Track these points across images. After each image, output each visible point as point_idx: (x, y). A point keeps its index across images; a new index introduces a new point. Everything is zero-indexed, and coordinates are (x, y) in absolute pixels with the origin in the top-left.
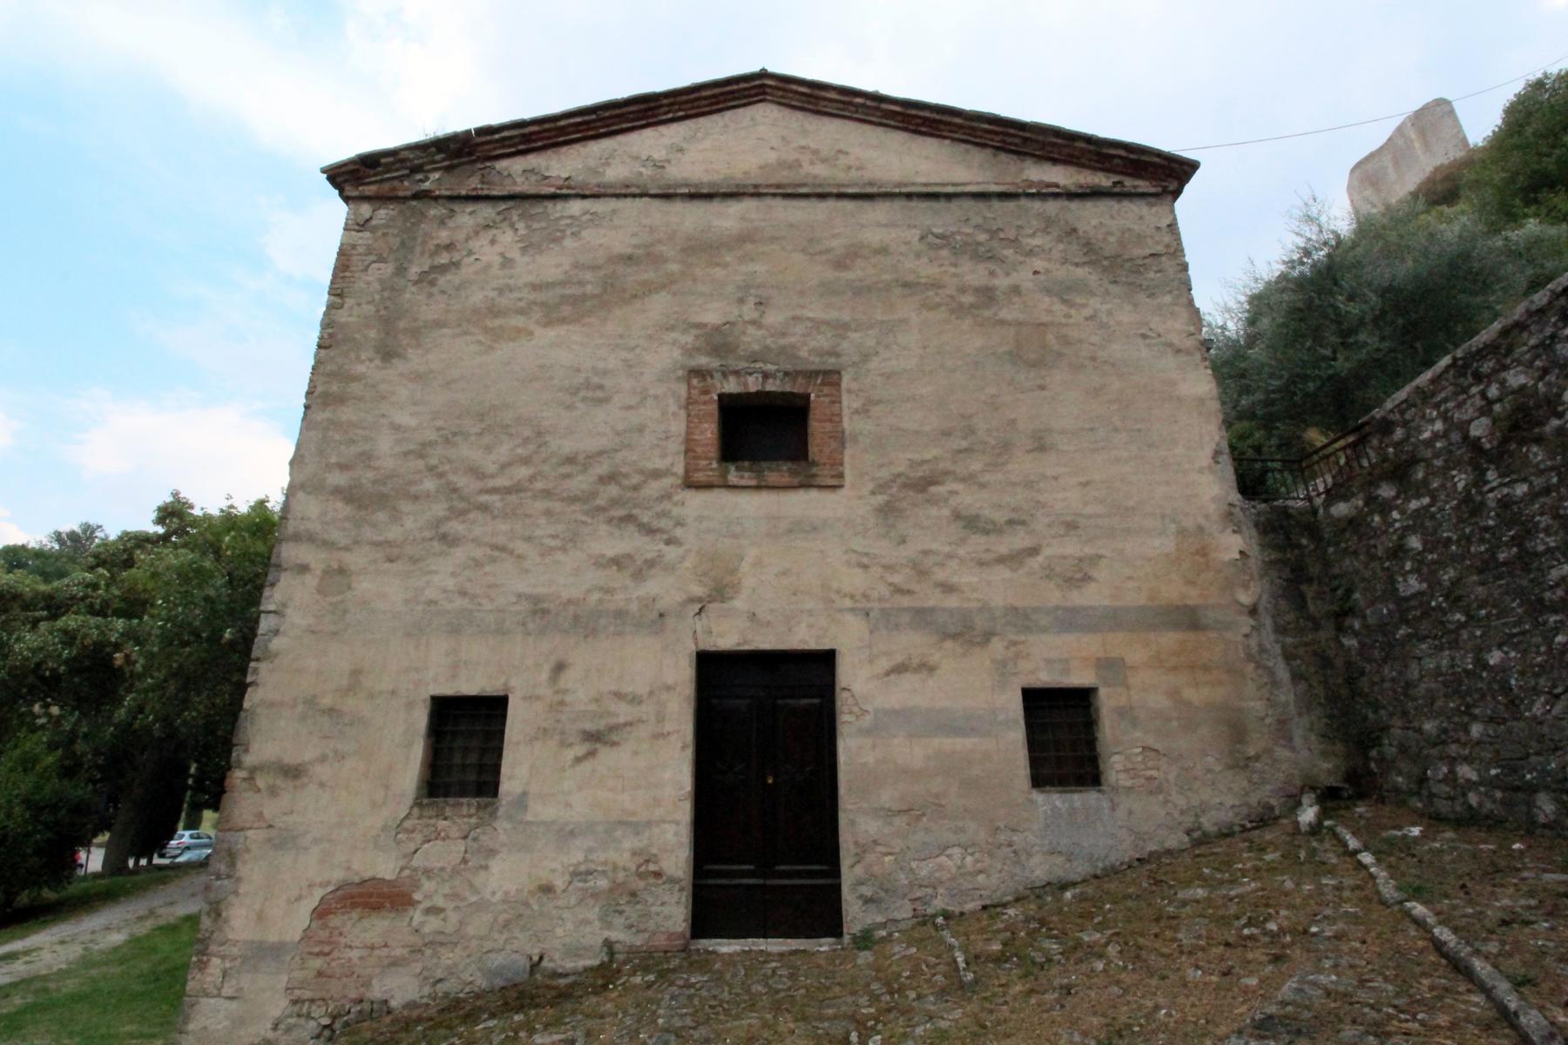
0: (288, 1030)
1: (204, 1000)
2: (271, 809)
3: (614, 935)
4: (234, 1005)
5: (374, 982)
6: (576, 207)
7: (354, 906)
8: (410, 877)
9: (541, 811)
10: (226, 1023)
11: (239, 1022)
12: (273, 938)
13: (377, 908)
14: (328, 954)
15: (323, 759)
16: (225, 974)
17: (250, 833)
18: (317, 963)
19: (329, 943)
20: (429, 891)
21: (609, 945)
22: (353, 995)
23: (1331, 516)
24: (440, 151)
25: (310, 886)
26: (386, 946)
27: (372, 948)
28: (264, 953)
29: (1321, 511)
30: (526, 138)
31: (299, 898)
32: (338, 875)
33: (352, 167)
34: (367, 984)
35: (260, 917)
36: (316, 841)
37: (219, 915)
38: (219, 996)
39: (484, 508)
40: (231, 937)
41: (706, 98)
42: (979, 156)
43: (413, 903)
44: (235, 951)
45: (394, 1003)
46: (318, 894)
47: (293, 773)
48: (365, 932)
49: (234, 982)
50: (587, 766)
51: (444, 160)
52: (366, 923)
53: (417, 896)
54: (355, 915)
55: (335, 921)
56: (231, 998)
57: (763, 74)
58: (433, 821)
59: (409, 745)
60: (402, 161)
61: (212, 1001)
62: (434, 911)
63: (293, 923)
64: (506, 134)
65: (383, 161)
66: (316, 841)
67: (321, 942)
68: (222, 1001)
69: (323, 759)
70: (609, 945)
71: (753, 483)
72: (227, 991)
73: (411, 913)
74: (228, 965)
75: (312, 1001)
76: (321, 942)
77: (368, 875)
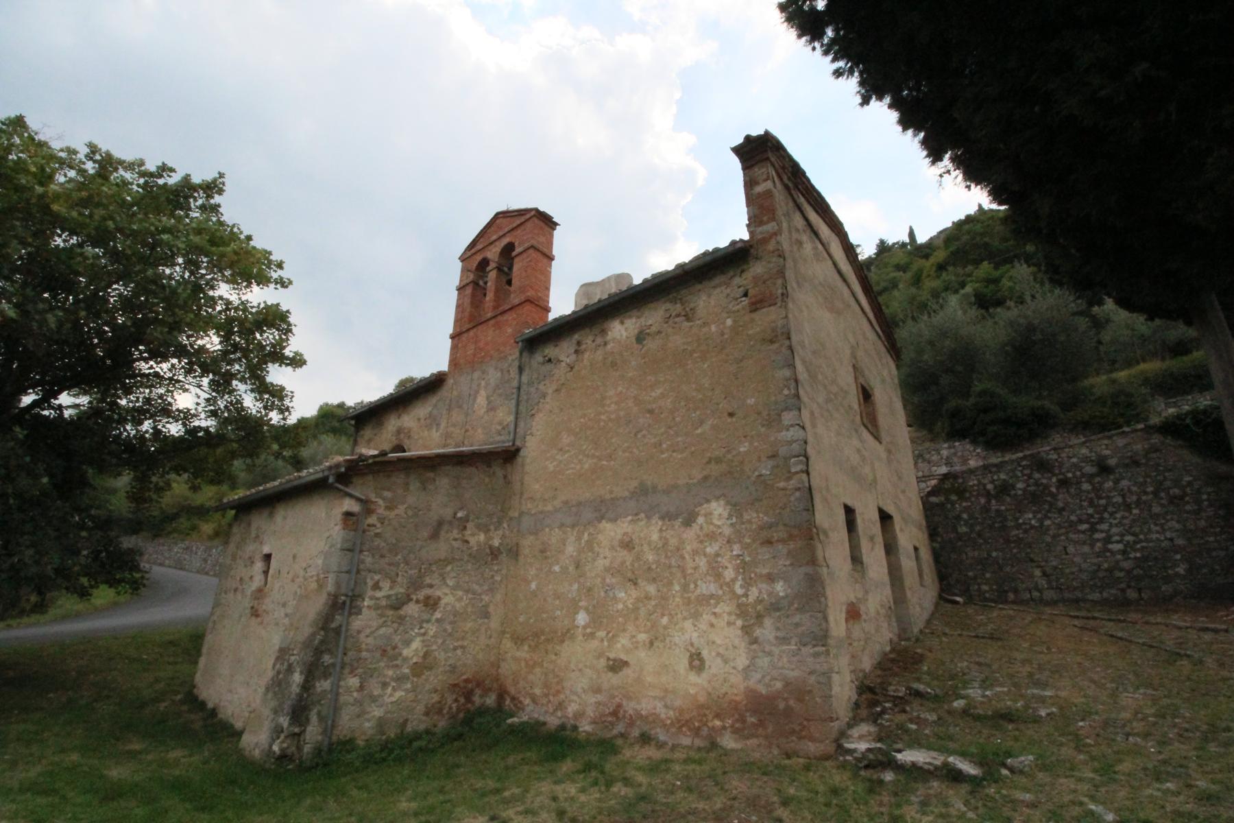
57: (841, 224)
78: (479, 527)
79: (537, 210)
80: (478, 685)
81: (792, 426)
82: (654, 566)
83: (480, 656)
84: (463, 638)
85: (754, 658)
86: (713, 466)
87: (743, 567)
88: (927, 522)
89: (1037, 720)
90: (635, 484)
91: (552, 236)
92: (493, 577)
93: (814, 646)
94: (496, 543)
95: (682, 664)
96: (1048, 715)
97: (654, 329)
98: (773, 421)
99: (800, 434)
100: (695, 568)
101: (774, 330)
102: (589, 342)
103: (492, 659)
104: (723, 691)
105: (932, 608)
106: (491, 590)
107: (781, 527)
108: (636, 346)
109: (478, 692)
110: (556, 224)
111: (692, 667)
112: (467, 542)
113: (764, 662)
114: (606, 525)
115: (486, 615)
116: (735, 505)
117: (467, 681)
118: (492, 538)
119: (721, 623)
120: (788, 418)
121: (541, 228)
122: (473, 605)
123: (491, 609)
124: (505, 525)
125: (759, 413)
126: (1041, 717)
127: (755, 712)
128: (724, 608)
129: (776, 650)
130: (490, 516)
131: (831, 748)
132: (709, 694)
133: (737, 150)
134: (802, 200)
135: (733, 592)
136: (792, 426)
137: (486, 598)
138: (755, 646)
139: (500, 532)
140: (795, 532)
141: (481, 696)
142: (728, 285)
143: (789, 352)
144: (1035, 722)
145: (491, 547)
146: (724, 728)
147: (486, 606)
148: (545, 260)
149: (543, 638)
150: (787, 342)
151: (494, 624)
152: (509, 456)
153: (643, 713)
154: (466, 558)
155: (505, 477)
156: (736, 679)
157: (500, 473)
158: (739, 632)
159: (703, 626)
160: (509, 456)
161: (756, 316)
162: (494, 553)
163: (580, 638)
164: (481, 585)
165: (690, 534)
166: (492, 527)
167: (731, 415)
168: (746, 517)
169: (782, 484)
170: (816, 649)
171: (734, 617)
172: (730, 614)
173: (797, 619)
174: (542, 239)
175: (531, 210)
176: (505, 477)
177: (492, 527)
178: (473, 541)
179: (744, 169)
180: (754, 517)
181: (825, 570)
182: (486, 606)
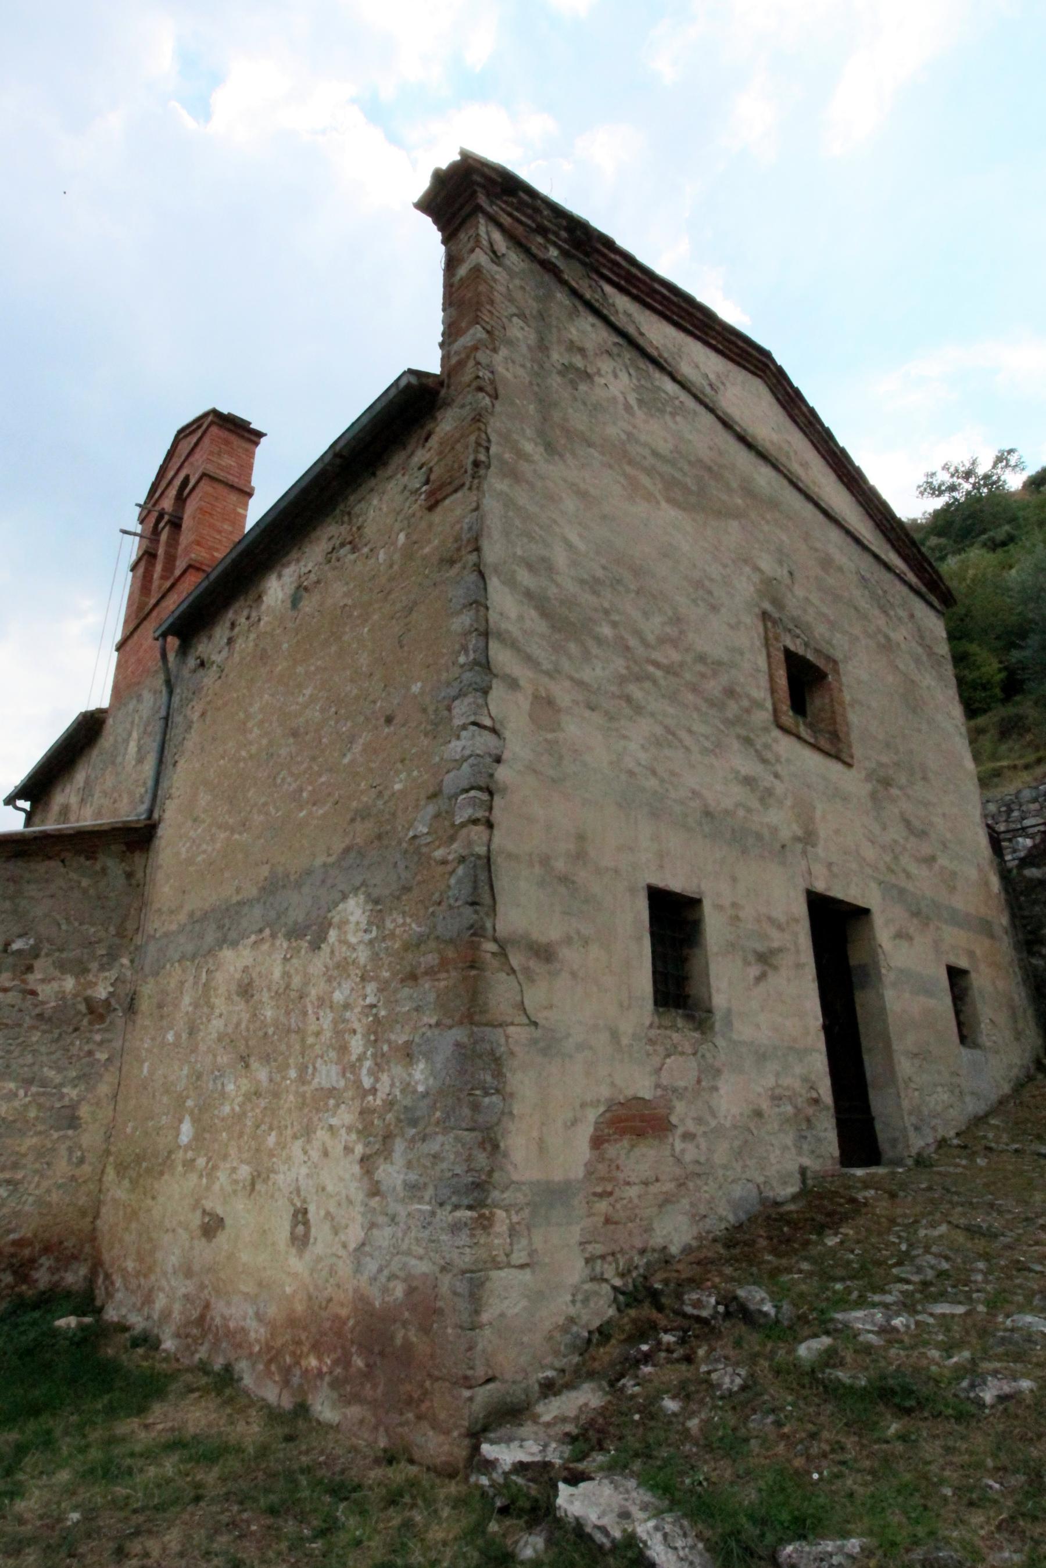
0: (586, 1301)
1: (494, 1274)
2: (534, 997)
3: (806, 1161)
4: (526, 1276)
5: (655, 1225)
6: (670, 387)
7: (623, 1132)
8: (662, 1096)
9: (743, 1031)
10: (524, 1303)
11: (537, 1297)
12: (558, 1176)
13: (640, 1134)
14: (611, 1194)
15: (568, 940)
16: (513, 1232)
17: (511, 1030)
18: (602, 1206)
19: (610, 1179)
20: (681, 1113)
21: (803, 1171)
22: (639, 1244)
23: (1025, 877)
24: (567, 229)
25: (583, 1105)
26: (657, 1180)
27: (646, 1184)
28: (553, 1195)
29: (1015, 871)
30: (629, 277)
31: (574, 1122)
32: (605, 1092)
33: (494, 176)
34: (648, 1230)
35: (542, 1146)
36: (580, 1047)
37: (496, 1147)
38: (509, 1265)
39: (649, 677)
40: (515, 1177)
41: (738, 347)
42: (870, 524)
43: (670, 1127)
44: (521, 1198)
45: (674, 1250)
46: (592, 1115)
47: (545, 953)
48: (640, 1160)
49: (524, 1242)
50: (762, 987)
51: (565, 241)
52: (637, 1152)
53: (674, 1119)
54: (625, 1143)
55: (611, 1150)
56: (522, 1267)
57: (767, 354)
58: (668, 1032)
59: (639, 939)
60: (537, 210)
61: (502, 1274)
62: (688, 1136)
63: (572, 1156)
64: (618, 258)
65: (522, 194)
66: (580, 1047)
67: (602, 1179)
68: (513, 1271)
69: (568, 940)
70: (803, 1171)
71: (812, 741)
72: (519, 1257)
73: (671, 1140)
74: (515, 1219)
75: (603, 1257)
76: (602, 1179)
77: (630, 1093)
78: (63, 967)
79: (214, 412)
80: (47, 1250)
81: (464, 727)
82: (271, 1031)
83: (55, 1197)
84: (15, 1166)
85: (373, 1225)
86: (359, 826)
87: (377, 1030)
88: (1013, 916)
89: (967, 1413)
90: (265, 871)
91: (251, 455)
92: (90, 1053)
93: (456, 1207)
94: (101, 992)
95: (282, 1229)
96: (1002, 1398)
97: (313, 577)
98: (439, 726)
99: (484, 742)
100: (317, 1034)
101: (457, 539)
102: (243, 620)
103: (83, 1200)
104: (326, 1294)
105: (1007, 1088)
106: (83, 1077)
107: (432, 944)
108: (290, 613)
109: (46, 1262)
110: (260, 435)
111: (294, 1238)
112: (33, 993)
113: (384, 1236)
114: (226, 953)
115: (73, 1121)
116: (376, 902)
117: (19, 1243)
118: (92, 985)
119: (337, 1150)
120: (461, 712)
121: (227, 442)
122: (40, 1107)
123: (84, 1111)
124: (125, 961)
125: (424, 710)
126: (980, 1404)
127: (366, 1349)
128: (345, 1116)
129: (402, 1211)
130: (90, 944)
131: (461, 1453)
132: (310, 1298)
133: (430, 205)
134: (622, 303)
135: (358, 1084)
136: (464, 727)
137: (71, 1092)
138: (374, 1202)
139: (112, 974)
140: (451, 954)
141: (52, 1271)
142: (404, 469)
143: (474, 577)
144: (960, 1417)
145: (88, 1001)
146: (320, 1375)
147: (74, 1106)
148: (233, 497)
149: (144, 1166)
150: (473, 558)
151: (90, 1137)
152: (138, 838)
153: (232, 1325)
154: (28, 1021)
155: (129, 875)
156: (345, 1268)
157: (115, 868)
158: (356, 1169)
159: (315, 1155)
160: (138, 838)
161: (437, 517)
162: (97, 1012)
163: (180, 1168)
164: (60, 1070)
165: (318, 964)
166: (94, 966)
167: (389, 720)
168: (389, 925)
169: (439, 854)
170: (458, 1214)
171: (354, 1136)
172: (349, 1129)
173: (433, 1146)
174: (227, 461)
175: (206, 415)
176: (129, 875)
177: (94, 966)
178: (46, 992)
179: (445, 242)
180: (403, 924)
181: (518, 1033)
182: (74, 1106)
